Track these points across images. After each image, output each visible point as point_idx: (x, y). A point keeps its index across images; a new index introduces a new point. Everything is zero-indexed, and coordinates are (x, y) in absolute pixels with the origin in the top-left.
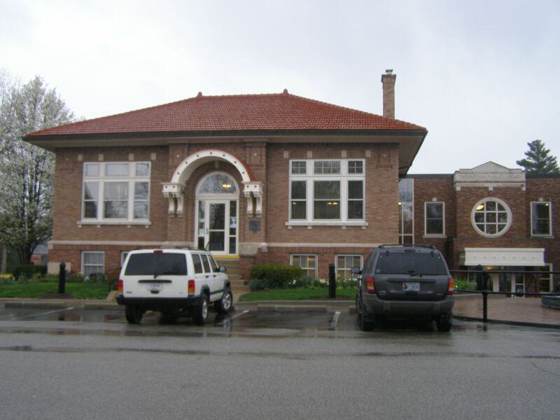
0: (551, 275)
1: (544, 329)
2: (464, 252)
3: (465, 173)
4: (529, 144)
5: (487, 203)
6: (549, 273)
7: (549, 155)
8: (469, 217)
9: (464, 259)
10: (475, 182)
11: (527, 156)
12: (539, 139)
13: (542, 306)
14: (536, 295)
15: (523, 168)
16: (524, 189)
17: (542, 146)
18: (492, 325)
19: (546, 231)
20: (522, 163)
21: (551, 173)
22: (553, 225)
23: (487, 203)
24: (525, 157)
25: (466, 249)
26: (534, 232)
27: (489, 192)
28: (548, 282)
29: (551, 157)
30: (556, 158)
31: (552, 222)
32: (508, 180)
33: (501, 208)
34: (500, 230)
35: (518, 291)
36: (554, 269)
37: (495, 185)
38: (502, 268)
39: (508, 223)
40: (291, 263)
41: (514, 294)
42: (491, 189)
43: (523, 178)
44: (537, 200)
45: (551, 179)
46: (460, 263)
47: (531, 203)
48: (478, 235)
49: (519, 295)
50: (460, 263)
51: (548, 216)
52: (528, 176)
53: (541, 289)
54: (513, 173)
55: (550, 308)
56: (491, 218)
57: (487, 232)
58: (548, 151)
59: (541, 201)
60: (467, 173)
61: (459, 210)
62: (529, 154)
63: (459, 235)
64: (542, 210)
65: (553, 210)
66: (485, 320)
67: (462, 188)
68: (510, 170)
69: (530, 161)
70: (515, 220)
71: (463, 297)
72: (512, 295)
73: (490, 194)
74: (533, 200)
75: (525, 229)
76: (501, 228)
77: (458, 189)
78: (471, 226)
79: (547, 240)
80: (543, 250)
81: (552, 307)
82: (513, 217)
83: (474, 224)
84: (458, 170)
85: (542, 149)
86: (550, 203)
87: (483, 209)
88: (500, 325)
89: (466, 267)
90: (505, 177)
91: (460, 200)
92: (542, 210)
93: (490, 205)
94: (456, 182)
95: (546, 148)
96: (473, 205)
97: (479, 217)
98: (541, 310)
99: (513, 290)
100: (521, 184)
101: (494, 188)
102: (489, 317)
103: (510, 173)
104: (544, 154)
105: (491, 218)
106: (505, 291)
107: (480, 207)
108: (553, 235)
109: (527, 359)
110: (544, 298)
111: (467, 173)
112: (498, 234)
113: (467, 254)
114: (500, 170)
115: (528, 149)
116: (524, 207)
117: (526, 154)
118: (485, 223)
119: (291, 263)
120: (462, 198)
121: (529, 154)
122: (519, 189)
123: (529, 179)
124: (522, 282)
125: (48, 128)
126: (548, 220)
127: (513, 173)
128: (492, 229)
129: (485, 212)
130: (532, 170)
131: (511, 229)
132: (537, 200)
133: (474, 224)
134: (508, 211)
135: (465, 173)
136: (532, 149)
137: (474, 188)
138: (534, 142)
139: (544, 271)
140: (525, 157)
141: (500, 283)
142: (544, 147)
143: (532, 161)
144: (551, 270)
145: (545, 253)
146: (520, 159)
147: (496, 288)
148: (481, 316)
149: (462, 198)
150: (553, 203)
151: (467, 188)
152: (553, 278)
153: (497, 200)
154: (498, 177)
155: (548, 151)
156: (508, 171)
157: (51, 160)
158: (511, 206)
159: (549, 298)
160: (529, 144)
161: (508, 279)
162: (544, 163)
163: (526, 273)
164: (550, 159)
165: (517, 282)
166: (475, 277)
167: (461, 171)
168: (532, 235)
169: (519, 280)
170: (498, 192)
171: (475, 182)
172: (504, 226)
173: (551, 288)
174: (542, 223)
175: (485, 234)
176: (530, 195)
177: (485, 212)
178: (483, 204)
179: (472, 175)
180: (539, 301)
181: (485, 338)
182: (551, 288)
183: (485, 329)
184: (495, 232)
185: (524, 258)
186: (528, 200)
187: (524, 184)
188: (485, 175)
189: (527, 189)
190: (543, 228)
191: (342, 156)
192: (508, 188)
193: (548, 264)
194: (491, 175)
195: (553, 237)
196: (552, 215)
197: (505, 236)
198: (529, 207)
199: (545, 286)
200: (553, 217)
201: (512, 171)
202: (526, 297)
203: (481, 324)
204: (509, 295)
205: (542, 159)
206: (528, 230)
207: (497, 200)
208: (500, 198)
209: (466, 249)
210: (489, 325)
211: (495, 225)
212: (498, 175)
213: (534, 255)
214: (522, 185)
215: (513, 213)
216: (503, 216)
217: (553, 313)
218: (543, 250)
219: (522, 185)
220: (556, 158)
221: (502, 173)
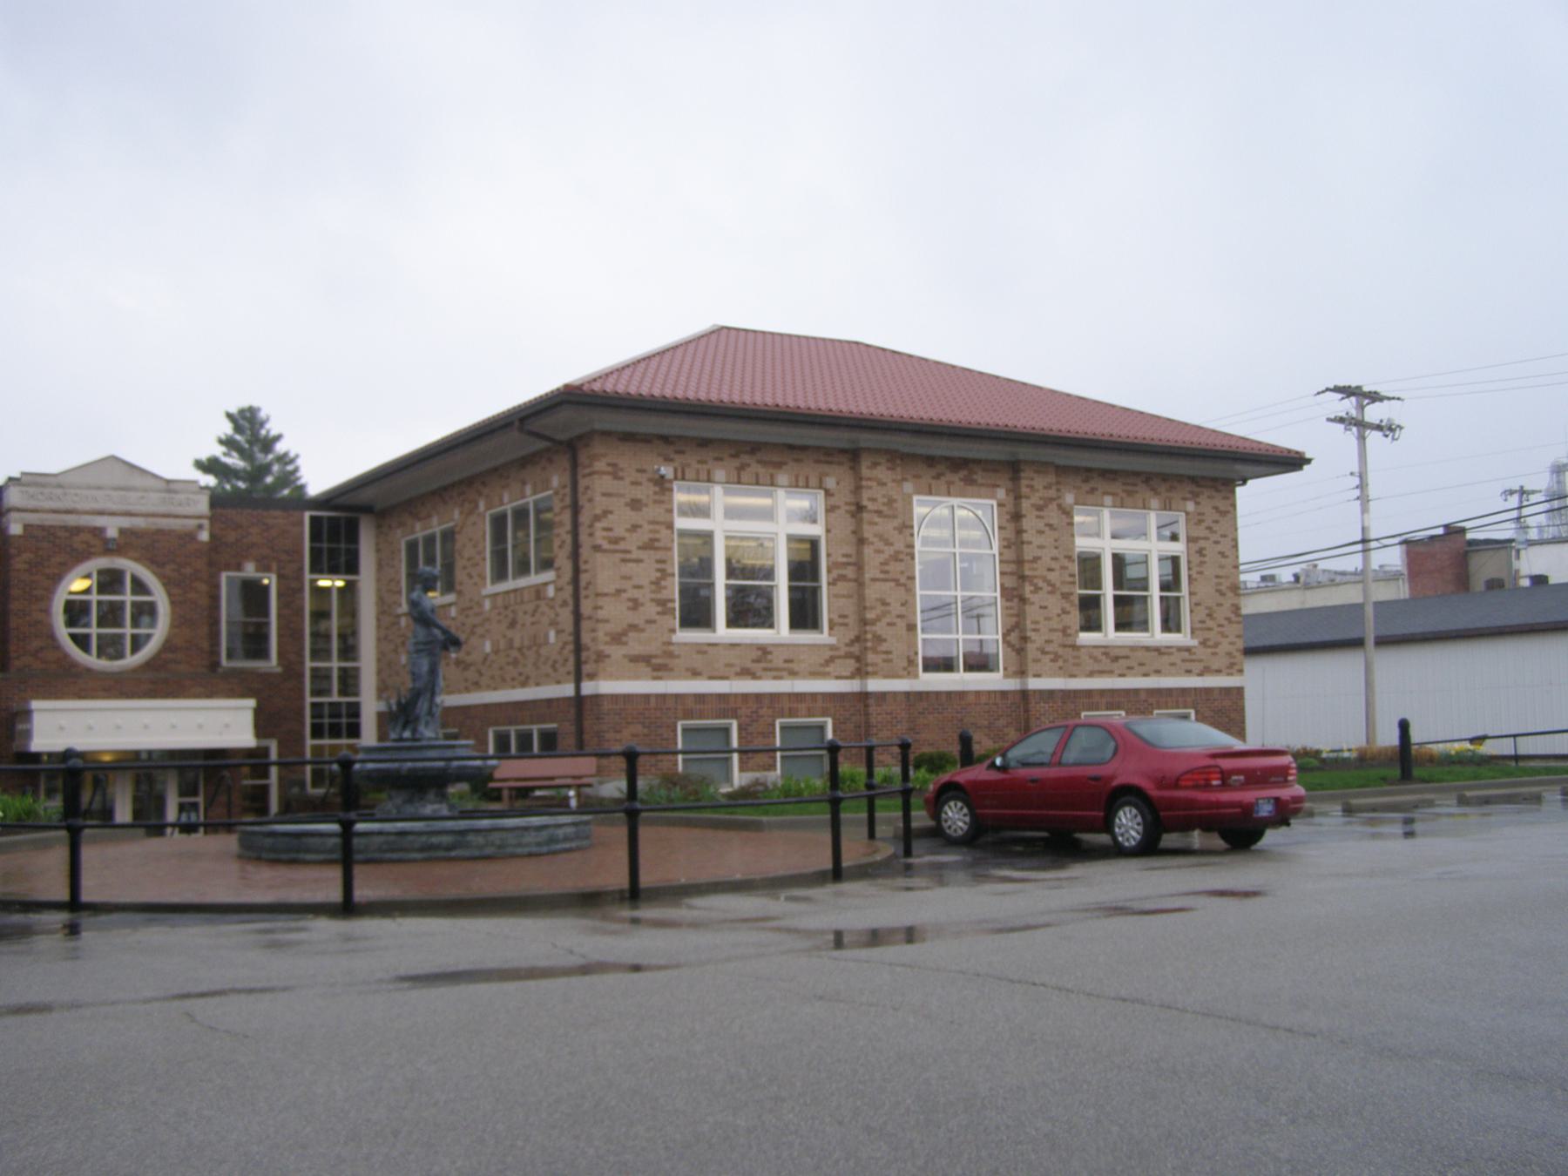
0: (274, 771)
1: (236, 917)
2: (27, 714)
3: (36, 484)
4: (229, 416)
5: (100, 572)
6: (268, 765)
7: (280, 447)
8: (47, 611)
9: (28, 734)
10: (68, 512)
11: (223, 449)
12: (255, 404)
13: (240, 857)
14: (229, 828)
15: (210, 480)
16: (204, 536)
17: (262, 424)
18: (92, 919)
19: (262, 653)
20: (209, 466)
21: (284, 499)
22: (280, 636)
23: (100, 572)
24: (218, 451)
25: (35, 704)
26: (230, 656)
27: (106, 541)
28: (265, 790)
29: (286, 454)
30: (297, 456)
31: (279, 628)
32: (162, 509)
33: (139, 586)
34: (136, 648)
35: (184, 818)
36: (280, 755)
37: (126, 522)
38: (144, 756)
39: (159, 632)
40: (680, 768)
41: (173, 825)
42: (112, 533)
43: (202, 505)
44: (239, 567)
45: (278, 513)
46: (16, 746)
47: (224, 577)
48: (74, 665)
49: (188, 828)
50: (16, 746)
51: (266, 613)
52: (217, 500)
53: (246, 811)
54: (175, 492)
55: (259, 859)
56: (111, 615)
57: (99, 656)
58: (278, 438)
59: (250, 570)
60: (43, 485)
61: (15, 592)
62: (228, 443)
63: (17, 663)
64: (253, 595)
65: (280, 595)
66: (74, 904)
67: (26, 527)
68: (168, 482)
69: (228, 461)
70: (178, 621)
71: (14, 845)
72: (169, 830)
73: (110, 548)
74: (228, 567)
75: (205, 645)
76: (137, 643)
77: (15, 529)
78: (52, 637)
79: (265, 677)
80: (251, 703)
81: (265, 855)
82: (173, 612)
83: (63, 632)
84: (16, 474)
85: (263, 432)
86: (274, 577)
87: (87, 591)
88: (115, 917)
89: (36, 757)
90: (154, 503)
91: (19, 563)
92: (253, 595)
93: (110, 581)
94: (10, 510)
95: (273, 428)
96: (57, 578)
97: (76, 611)
98: (234, 866)
99: (171, 814)
100: (194, 522)
101: (122, 531)
102: (86, 896)
103: (169, 491)
104: (268, 444)
105: (111, 615)
106: (149, 821)
107: (79, 585)
108: (279, 664)
109: (176, 1003)
110: (245, 833)
111: (43, 485)
112: (131, 661)
113: (38, 720)
114: (137, 481)
115: (227, 429)
116: (203, 587)
117: (221, 442)
118: (94, 631)
119: (680, 768)
120: (27, 556)
121: (228, 443)
122: (190, 536)
123: (219, 511)
124: (195, 793)
125: (1051, 478)
126: (267, 624)
127: (175, 492)
128: (111, 647)
129: (94, 598)
130: (235, 488)
131: (168, 646)
132: (239, 567)
133: (63, 632)
134: (160, 597)
135: (36, 484)
136: (238, 428)
137: (66, 528)
138: (242, 412)
139: (255, 760)
140: (218, 451)
141: (136, 800)
142: (268, 426)
143: (234, 461)
144: (274, 756)
145: (258, 713)
146: (204, 456)
147: (123, 812)
148: (63, 895)
149: (27, 556)
150: (280, 577)
151: (42, 528)
152: (281, 779)
153: (130, 566)
154: (134, 502)
155: (278, 438)
156: (164, 485)
157: (1036, 559)
158: (167, 583)
159: (254, 833)
160: (229, 416)
161: (159, 787)
162: (265, 469)
163: (206, 768)
164: (284, 459)
165: (182, 794)
166: (59, 783)
167: (25, 479)
168: (224, 662)
169: (188, 790)
170: (129, 542)
171: (68, 512)
172: (149, 637)
173: (274, 806)
174: (251, 630)
175: (91, 660)
176: (220, 554)
177: (94, 598)
178: (88, 576)
179: (59, 491)
180: (230, 842)
181: (74, 956)
182: (274, 806)
183: (73, 930)
184: (120, 655)
185: (200, 726)
186: (215, 567)
187: (206, 522)
188: (95, 493)
189: (212, 535)
190: (255, 643)
191: (1190, 544)
192: (160, 532)
193: (265, 742)
194: (114, 494)
195: (279, 670)
196: (279, 609)
197: (149, 665)
198: (217, 586)
199: (258, 800)
200: (280, 616)
201: (172, 486)
202: (206, 833)
203: (62, 917)
204: (158, 830)
205: (261, 458)
206: (214, 651)
207: (130, 566)
208: (136, 560)
209: (35, 704)
210: (85, 920)
211: (121, 637)
212: (133, 495)
213: (226, 717)
214: (200, 527)
215: (173, 603)
216: (145, 611)
217: (266, 873)
218: (251, 703)
219: (200, 527)
220: (297, 456)
221: (145, 490)
